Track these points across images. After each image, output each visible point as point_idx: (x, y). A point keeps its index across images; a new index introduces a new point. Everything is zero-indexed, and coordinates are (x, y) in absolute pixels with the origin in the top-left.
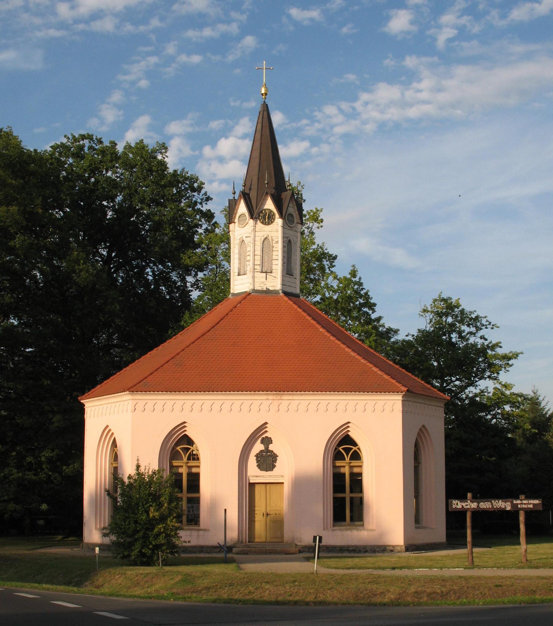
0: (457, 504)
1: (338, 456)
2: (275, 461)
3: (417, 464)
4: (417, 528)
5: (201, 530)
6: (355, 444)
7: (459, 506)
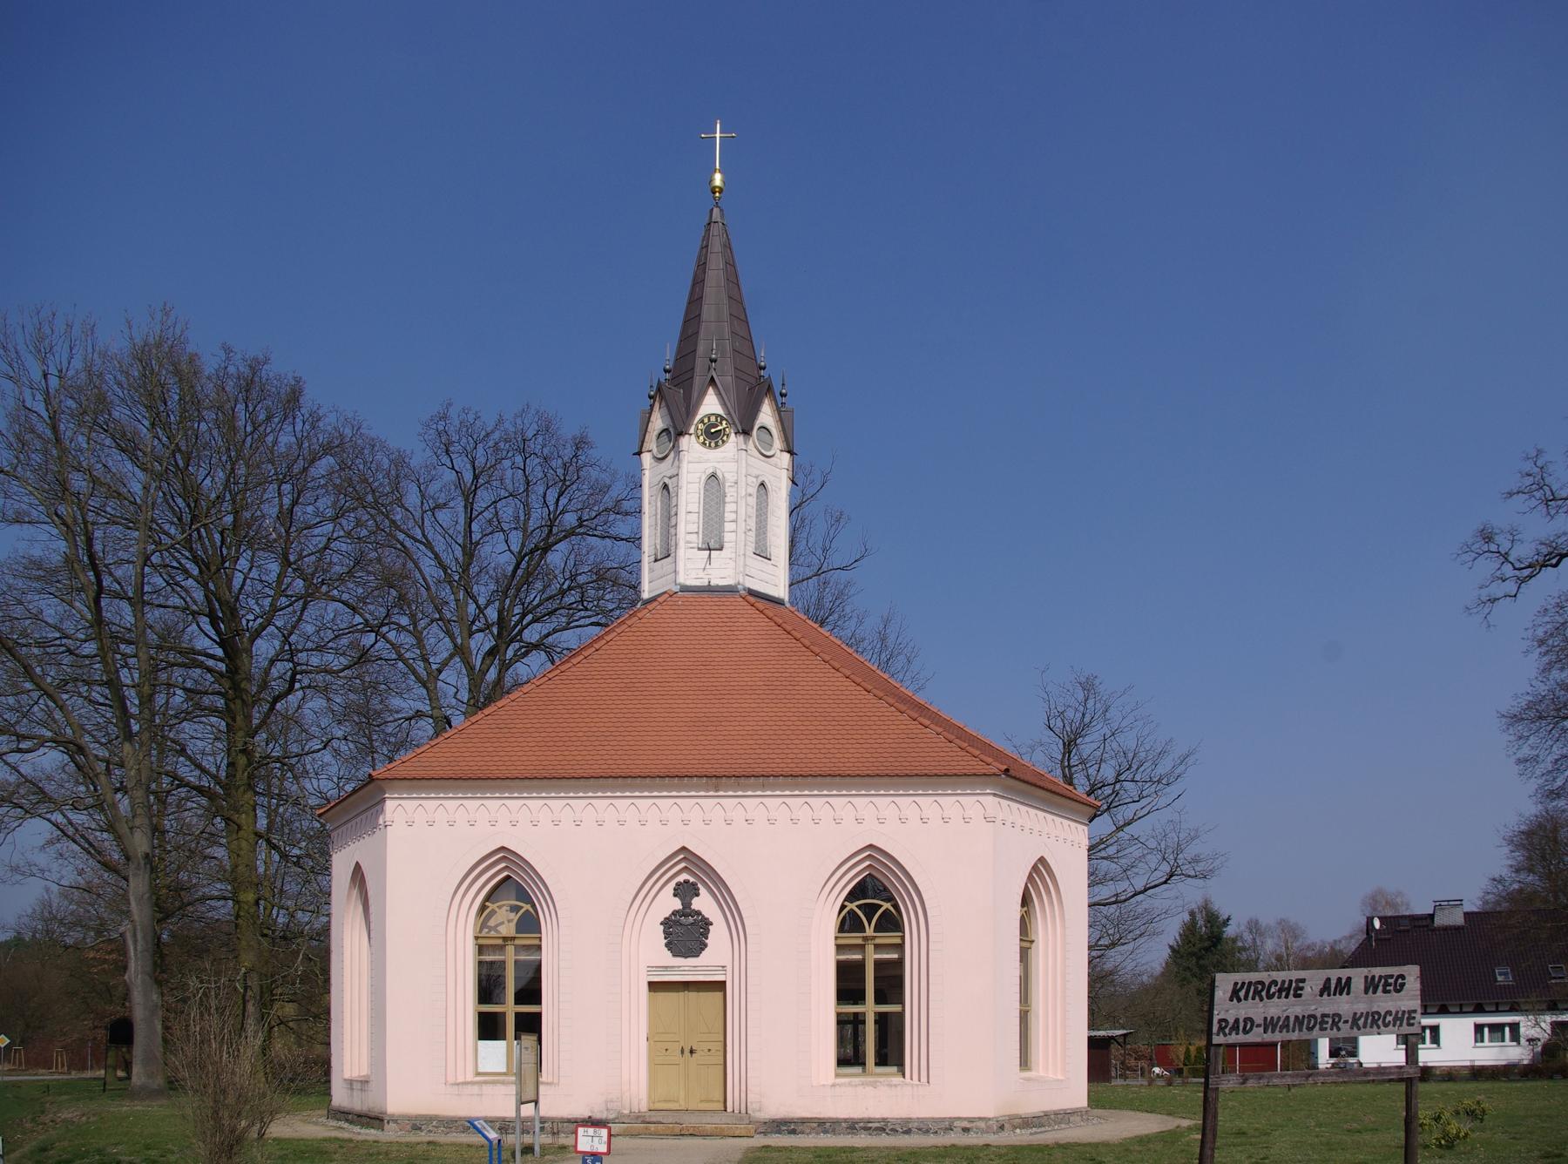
1: (849, 923)
3: (1026, 945)
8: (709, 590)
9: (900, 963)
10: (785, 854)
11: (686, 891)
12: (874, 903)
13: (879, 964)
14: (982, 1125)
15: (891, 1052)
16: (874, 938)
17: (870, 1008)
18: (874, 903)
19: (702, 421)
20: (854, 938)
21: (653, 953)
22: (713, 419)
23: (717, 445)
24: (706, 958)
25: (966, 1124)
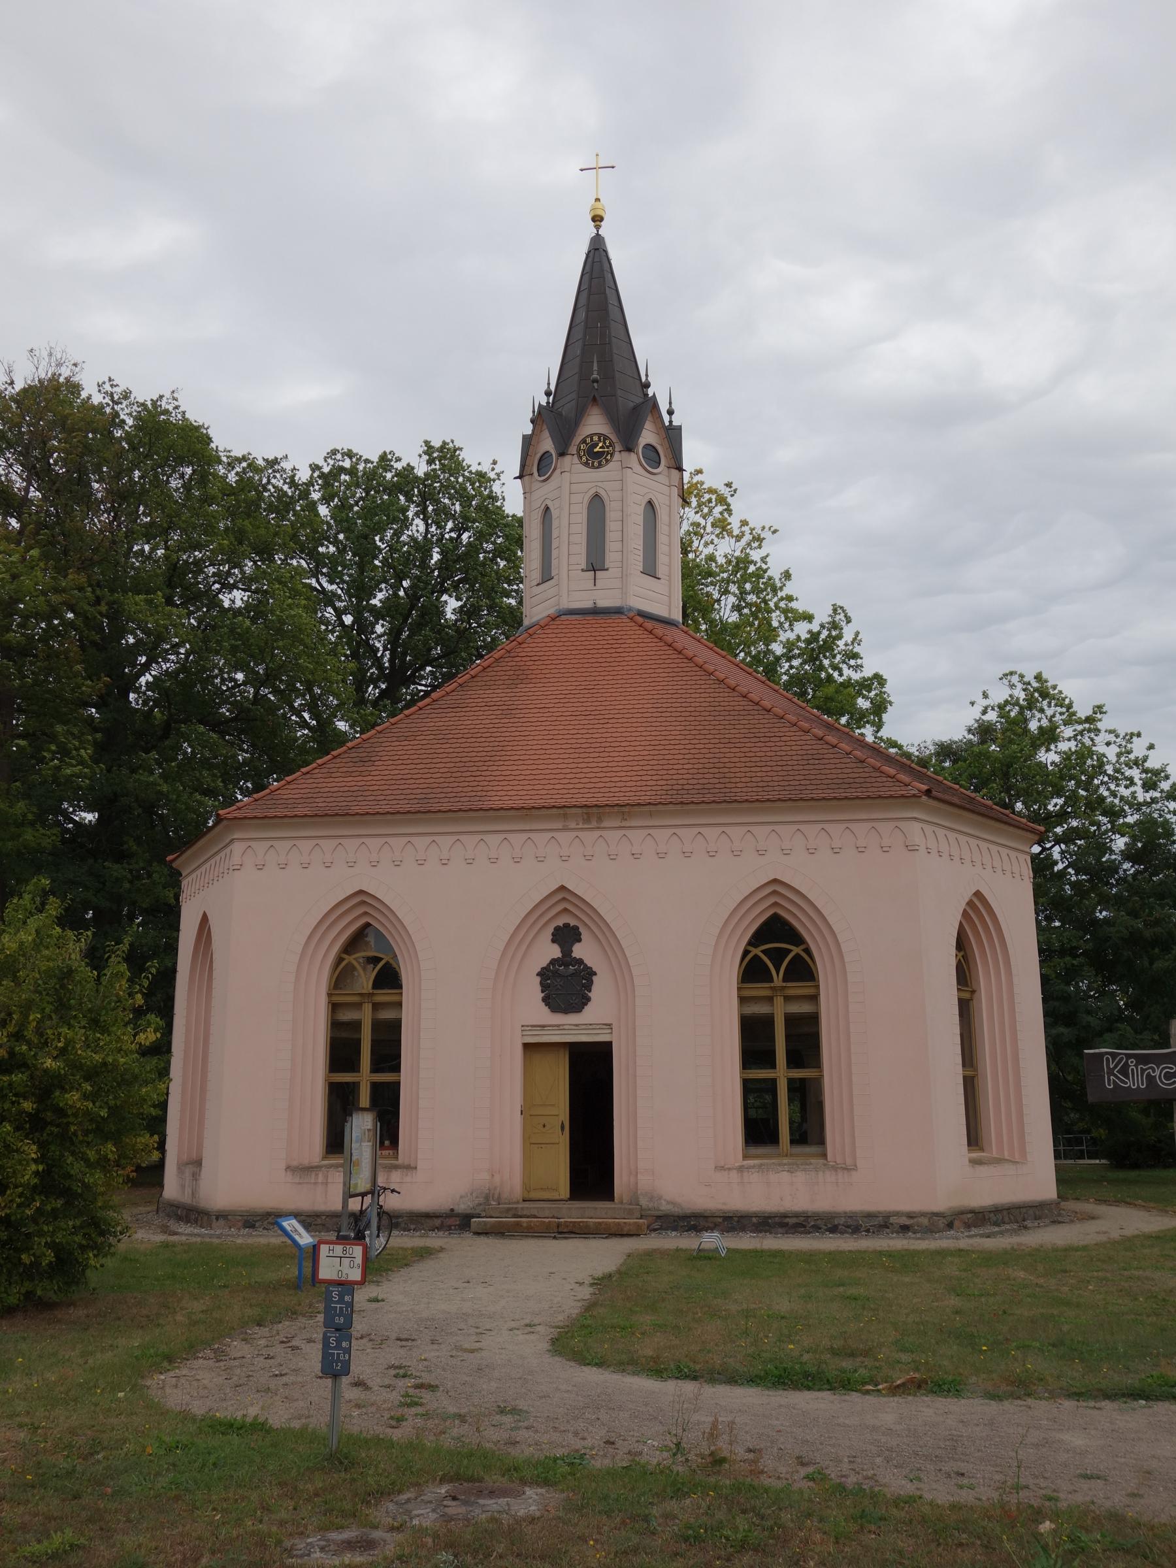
0: (1124, 1071)
1: (752, 971)
2: (589, 986)
3: (966, 996)
4: (974, 1162)
5: (396, 1167)
6: (796, 938)
7: (1136, 1082)
8: (595, 612)
9: (814, 1019)
10: (672, 909)
11: (566, 936)
12: (778, 951)
13: (790, 1020)
14: (925, 1221)
15: (809, 1132)
16: (783, 988)
17: (782, 1073)
18: (778, 951)
19: (584, 441)
20: (759, 989)
21: (531, 1008)
22: (596, 438)
23: (600, 466)
24: (589, 1014)
25: (904, 1221)
